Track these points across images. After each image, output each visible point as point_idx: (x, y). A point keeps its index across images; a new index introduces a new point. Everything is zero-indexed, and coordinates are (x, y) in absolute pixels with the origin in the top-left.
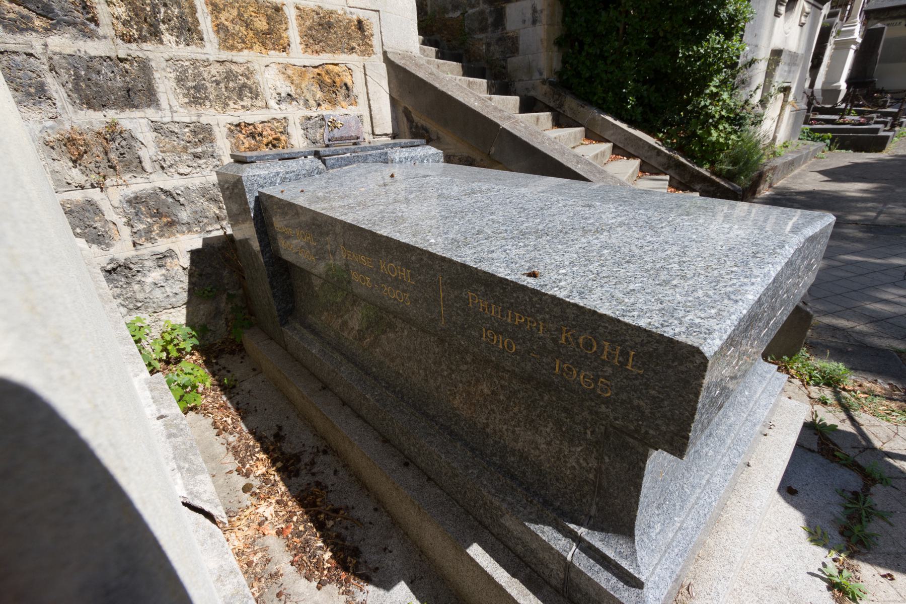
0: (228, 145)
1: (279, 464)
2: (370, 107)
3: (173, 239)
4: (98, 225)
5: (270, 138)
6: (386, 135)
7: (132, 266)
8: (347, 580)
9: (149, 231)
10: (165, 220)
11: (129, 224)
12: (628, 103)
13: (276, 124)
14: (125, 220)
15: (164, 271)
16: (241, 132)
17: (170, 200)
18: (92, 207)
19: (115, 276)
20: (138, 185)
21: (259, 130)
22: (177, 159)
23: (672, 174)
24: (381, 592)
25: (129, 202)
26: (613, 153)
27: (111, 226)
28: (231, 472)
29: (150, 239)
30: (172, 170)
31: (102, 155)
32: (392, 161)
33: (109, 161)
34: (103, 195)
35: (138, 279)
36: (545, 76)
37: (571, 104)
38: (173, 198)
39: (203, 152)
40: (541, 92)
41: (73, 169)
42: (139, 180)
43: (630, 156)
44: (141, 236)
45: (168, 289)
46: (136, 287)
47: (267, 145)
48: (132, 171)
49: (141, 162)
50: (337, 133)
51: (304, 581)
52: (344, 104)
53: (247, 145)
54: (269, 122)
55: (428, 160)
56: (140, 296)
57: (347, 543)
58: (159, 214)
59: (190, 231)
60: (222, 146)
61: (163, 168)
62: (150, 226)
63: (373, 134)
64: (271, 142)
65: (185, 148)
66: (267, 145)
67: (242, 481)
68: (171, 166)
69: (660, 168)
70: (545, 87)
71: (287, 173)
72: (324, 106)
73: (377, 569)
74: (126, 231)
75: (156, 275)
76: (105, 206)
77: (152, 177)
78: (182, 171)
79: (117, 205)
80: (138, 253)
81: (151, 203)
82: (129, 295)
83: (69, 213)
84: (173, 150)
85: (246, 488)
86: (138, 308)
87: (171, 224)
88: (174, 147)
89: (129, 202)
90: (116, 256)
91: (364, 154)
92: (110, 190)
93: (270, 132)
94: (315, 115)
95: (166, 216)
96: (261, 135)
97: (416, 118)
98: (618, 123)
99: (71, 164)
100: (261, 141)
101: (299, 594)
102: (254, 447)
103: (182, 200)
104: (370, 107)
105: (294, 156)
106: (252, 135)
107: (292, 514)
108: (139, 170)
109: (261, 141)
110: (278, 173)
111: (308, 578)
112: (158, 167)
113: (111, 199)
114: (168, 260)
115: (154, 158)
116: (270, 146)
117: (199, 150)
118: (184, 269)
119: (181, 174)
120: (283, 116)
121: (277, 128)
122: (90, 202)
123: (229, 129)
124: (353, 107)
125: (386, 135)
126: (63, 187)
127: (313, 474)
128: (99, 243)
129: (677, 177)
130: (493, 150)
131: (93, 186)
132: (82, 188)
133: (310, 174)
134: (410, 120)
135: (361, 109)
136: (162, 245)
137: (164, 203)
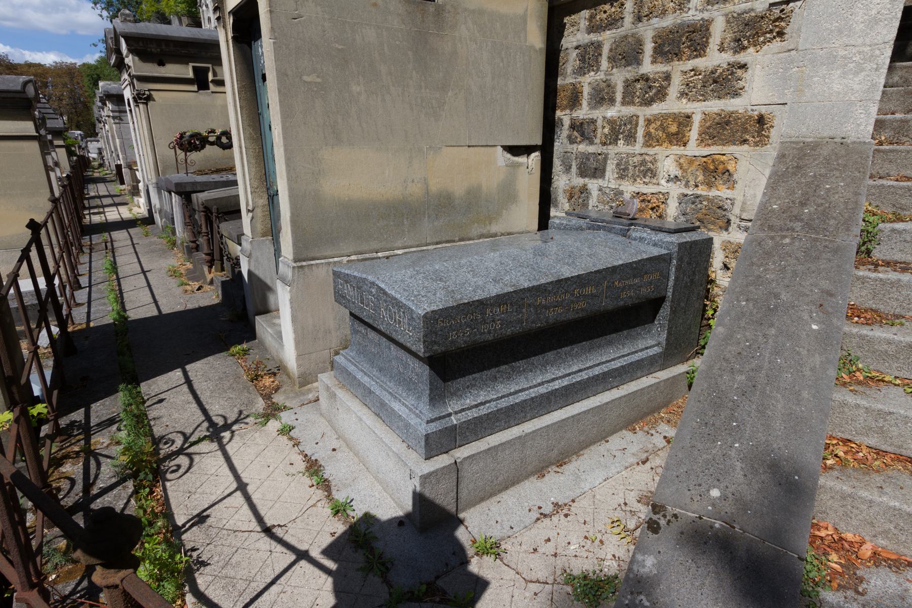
72: (700, 187)
96: (649, 201)
100: (647, 206)
124: (728, 191)
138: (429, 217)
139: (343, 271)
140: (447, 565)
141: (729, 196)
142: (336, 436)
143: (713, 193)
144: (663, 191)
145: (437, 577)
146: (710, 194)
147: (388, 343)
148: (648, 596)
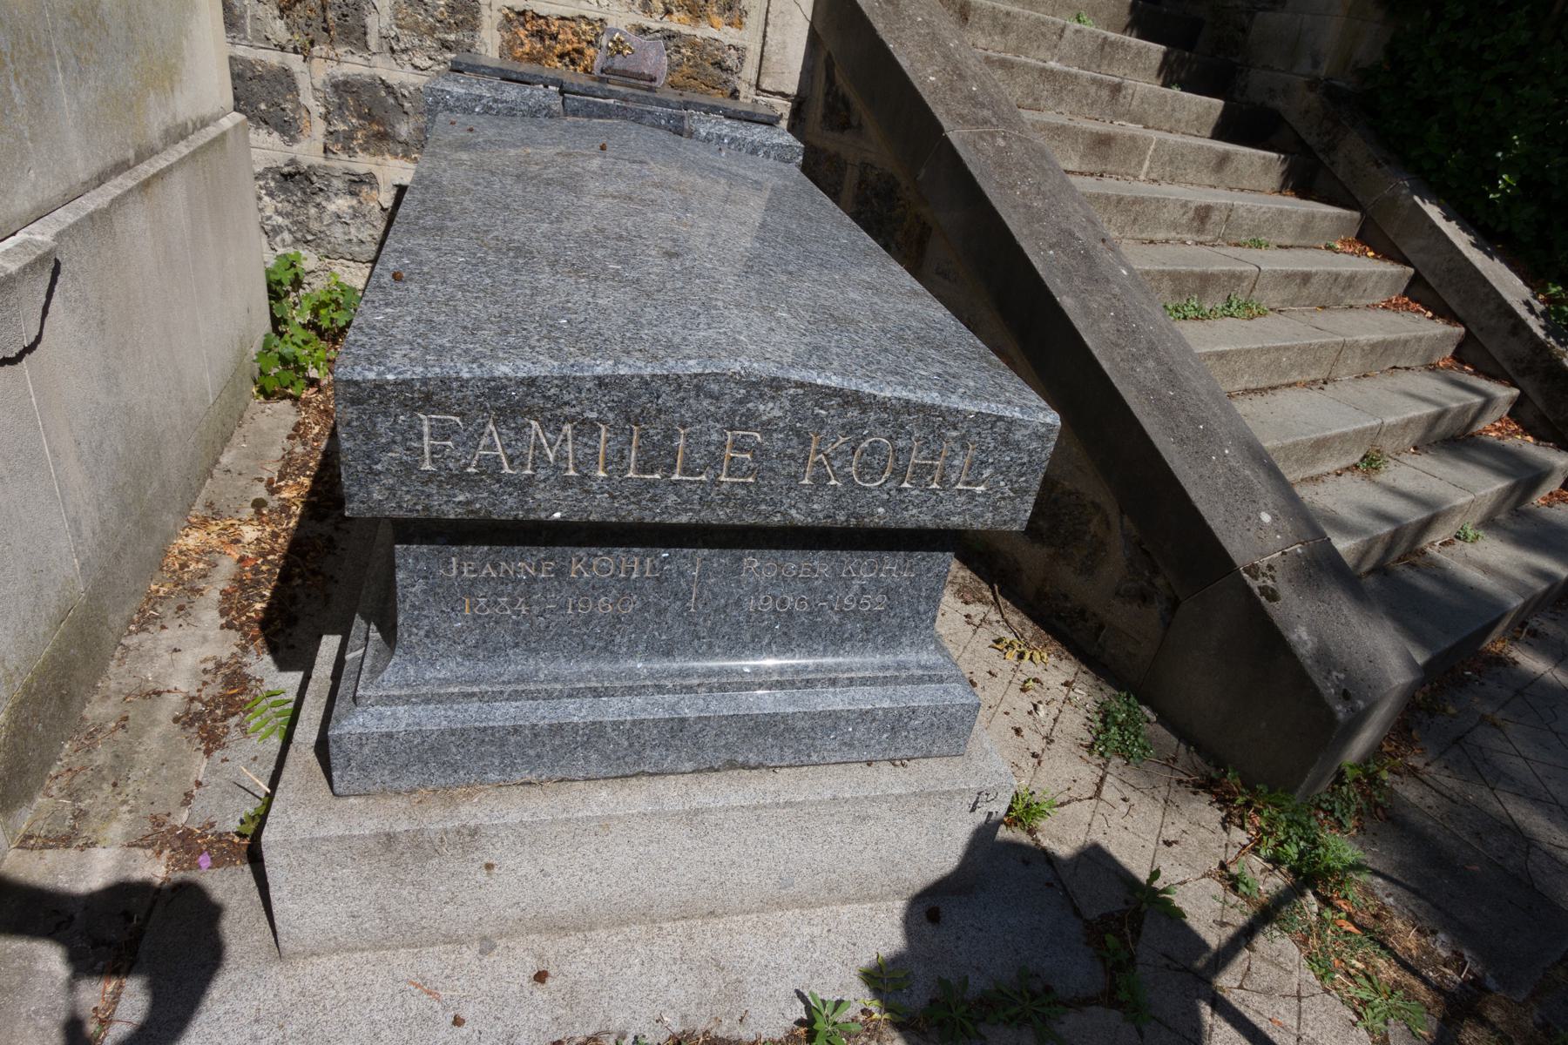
0: (498, 41)
1: (314, 499)
2: (764, 36)
3: (379, 159)
4: (288, 106)
5: (569, 47)
6: (784, 95)
7: (314, 179)
8: (254, 639)
9: (350, 136)
10: (376, 128)
11: (326, 118)
12: (1495, 188)
13: (583, 26)
14: (322, 110)
15: (354, 202)
16: (523, 25)
17: (391, 101)
18: (285, 79)
19: (291, 185)
20: (353, 66)
21: (554, 29)
22: (416, 42)
23: (1530, 392)
24: (273, 668)
25: (335, 86)
26: (1405, 294)
27: (304, 113)
28: (261, 480)
29: (347, 149)
30: (405, 57)
31: (319, 11)
32: (691, 135)
33: (325, 21)
34: (304, 67)
35: (318, 200)
36: (1323, 71)
37: (1354, 149)
38: (396, 98)
39: (457, 42)
40: (1299, 105)
41: (278, 21)
42: (356, 59)
43: (1442, 312)
44: (337, 141)
45: (353, 230)
46: (313, 211)
47: (561, 56)
48: (350, 44)
49: (365, 34)
50: (618, 62)
51: (216, 614)
52: (717, 20)
53: (527, 48)
54: (573, 20)
55: (767, 155)
56: (314, 226)
57: (293, 609)
58: (369, 117)
59: (406, 156)
60: (488, 40)
61: (392, 50)
62: (354, 129)
63: (758, 86)
64: (568, 54)
65: (432, 29)
66: (561, 56)
67: (261, 492)
68: (405, 51)
69: (1506, 366)
70: (1312, 96)
71: (495, 101)
72: (676, 15)
73: (293, 647)
74: (319, 128)
75: (342, 204)
76: (303, 83)
77: (376, 59)
78: (417, 61)
79: (318, 86)
80: (328, 163)
81: (365, 97)
82: (301, 218)
83: (236, 77)
84: (414, 28)
85: (258, 504)
86: (307, 242)
87: (383, 137)
88: (417, 23)
89: (335, 86)
90: (299, 157)
91: (640, 107)
92: (316, 62)
93: (570, 36)
94: (656, 26)
95: (378, 124)
96: (554, 37)
97: (839, 80)
98: (1451, 229)
99: (277, 13)
100: (551, 48)
101: (199, 620)
102: (310, 469)
103: (407, 105)
104: (764, 36)
105: (527, 79)
106: (539, 35)
107: (273, 551)
108: (360, 44)
109: (551, 48)
110: (481, 97)
111: (223, 613)
112: (386, 47)
113: (314, 75)
114: (366, 189)
115: (384, 32)
116: (567, 60)
117: (452, 37)
118: (383, 209)
119: (416, 67)
120: (599, 15)
121: (584, 33)
122: (287, 73)
123: (506, 16)
124: (732, 31)
125: (784, 95)
126: (260, 40)
127: (337, 529)
128: (283, 132)
129: (1539, 403)
130: (923, 172)
131: (295, 51)
132: (283, 49)
133: (533, 113)
134: (830, 80)
135: (748, 37)
136: (362, 163)
137: (382, 101)
138: (64, 69)
139: (503, 369)
140: (1050, 885)
141: (734, 42)
142: (469, 954)
143: (703, 31)
144: (590, 15)
145: (1077, 912)
146: (698, 33)
147: (721, 559)
148: (1413, 662)
